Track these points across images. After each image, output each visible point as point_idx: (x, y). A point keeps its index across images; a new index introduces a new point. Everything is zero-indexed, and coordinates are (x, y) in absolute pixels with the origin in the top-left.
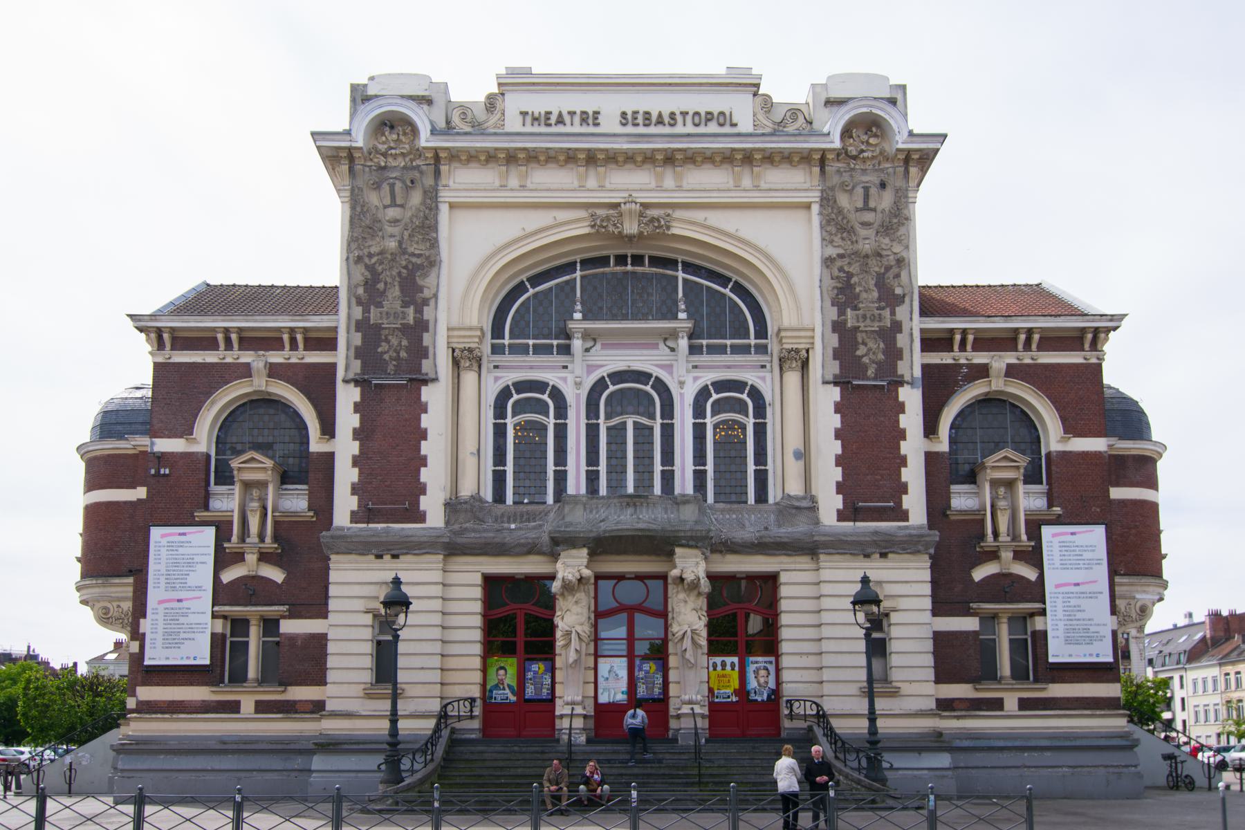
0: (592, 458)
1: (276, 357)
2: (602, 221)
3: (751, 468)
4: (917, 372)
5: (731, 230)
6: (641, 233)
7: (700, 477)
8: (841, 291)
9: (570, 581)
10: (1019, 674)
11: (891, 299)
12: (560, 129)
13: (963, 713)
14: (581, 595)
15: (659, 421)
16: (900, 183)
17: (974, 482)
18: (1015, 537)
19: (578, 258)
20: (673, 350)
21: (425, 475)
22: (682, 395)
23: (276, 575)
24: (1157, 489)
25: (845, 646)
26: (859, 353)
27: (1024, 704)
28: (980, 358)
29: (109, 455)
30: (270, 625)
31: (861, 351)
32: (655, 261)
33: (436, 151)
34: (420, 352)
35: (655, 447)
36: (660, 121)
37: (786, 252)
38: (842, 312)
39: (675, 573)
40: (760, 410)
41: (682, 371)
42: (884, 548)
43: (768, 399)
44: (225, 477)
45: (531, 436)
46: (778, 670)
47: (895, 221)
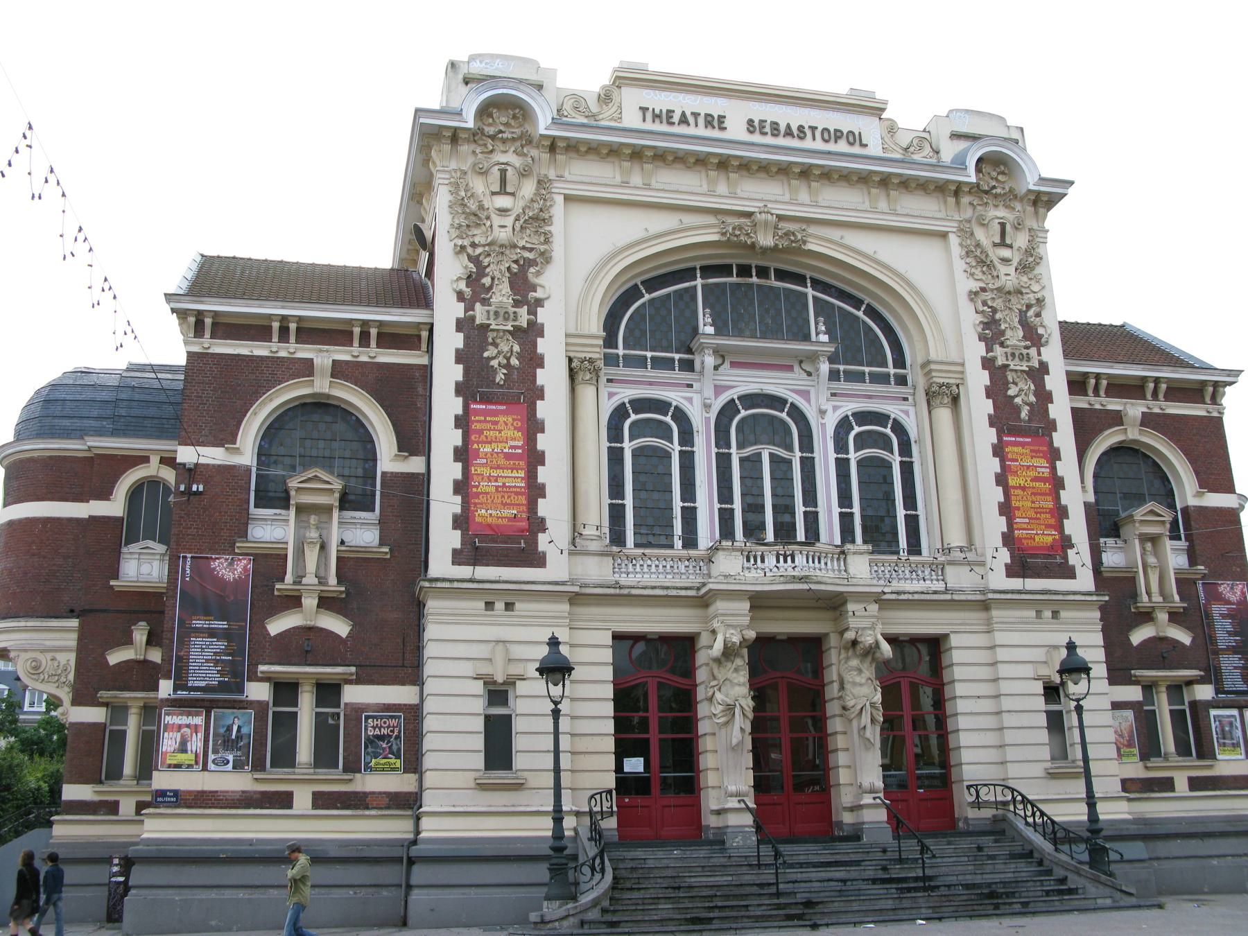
0: (725, 493)
2: (734, 229)
6: (776, 245)
8: (986, 325)
9: (734, 644)
11: (1034, 338)
12: (682, 130)
13: (1138, 795)
19: (698, 264)
20: (809, 374)
22: (823, 425)
23: (339, 626)
25: (1025, 720)
26: (1010, 393)
29: (50, 457)
30: (328, 692)
36: (788, 133)
37: (931, 281)
40: (905, 449)
41: (822, 400)
43: (913, 434)
46: (557, 770)
47: (1031, 259)
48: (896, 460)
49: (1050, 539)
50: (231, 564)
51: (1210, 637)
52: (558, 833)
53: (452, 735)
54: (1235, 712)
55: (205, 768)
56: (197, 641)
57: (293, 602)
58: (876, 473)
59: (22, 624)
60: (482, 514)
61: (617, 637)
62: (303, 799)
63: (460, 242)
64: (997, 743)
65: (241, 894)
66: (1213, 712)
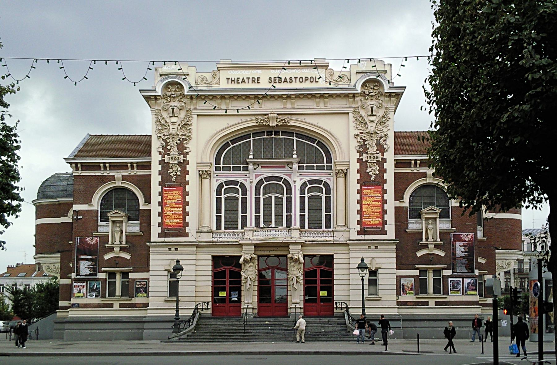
0: (257, 210)
1: (125, 173)
3: (324, 213)
5: (315, 123)
15: (285, 196)
17: (420, 218)
19: (229, 141)
20: (291, 168)
22: (295, 186)
23: (128, 256)
24: (521, 214)
26: (367, 171)
28: (423, 170)
30: (125, 275)
36: (285, 81)
37: (341, 132)
39: (289, 256)
40: (328, 191)
44: (104, 218)
45: (231, 202)
48: (324, 196)
49: (378, 222)
50: (92, 239)
51: (453, 253)
54: (461, 279)
55: (86, 297)
56: (82, 262)
57: (111, 249)
58: (315, 201)
59: (43, 256)
60: (168, 222)
61: (213, 257)
62: (116, 305)
63: (159, 135)
64: (347, 289)
65: (98, 331)
66: (450, 279)
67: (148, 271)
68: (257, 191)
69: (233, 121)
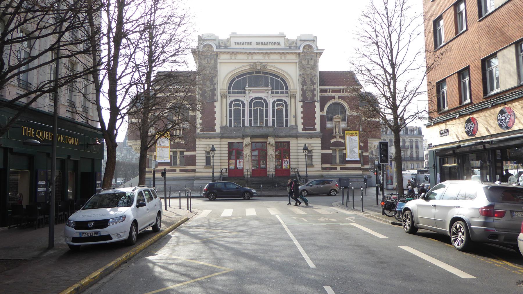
0: (250, 116)
1: (339, 95)
3: (284, 118)
4: (319, 99)
7: (273, 120)
8: (303, 82)
10: (341, 162)
14: (249, 147)
16: (315, 58)
18: (340, 134)
21: (216, 121)
27: (341, 169)
28: (333, 94)
30: (182, 153)
31: (307, 95)
32: (264, 73)
33: (217, 52)
34: (214, 95)
35: (264, 114)
37: (291, 72)
38: (303, 86)
39: (268, 142)
40: (286, 106)
42: (311, 136)
45: (237, 112)
48: (284, 108)
52: (213, 175)
53: (201, 160)
58: (280, 112)
67: (195, 151)
68: (250, 106)
69: (239, 65)
